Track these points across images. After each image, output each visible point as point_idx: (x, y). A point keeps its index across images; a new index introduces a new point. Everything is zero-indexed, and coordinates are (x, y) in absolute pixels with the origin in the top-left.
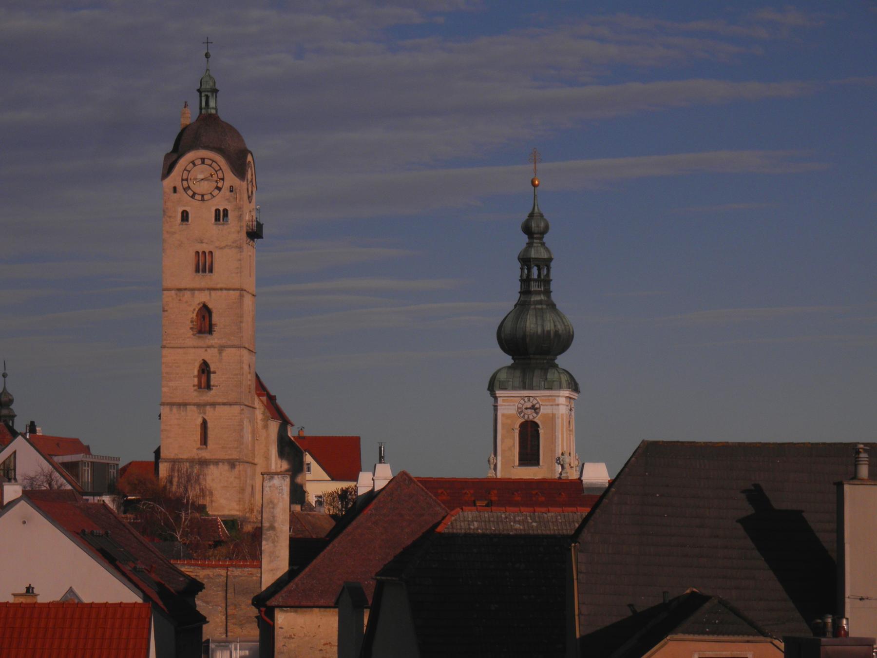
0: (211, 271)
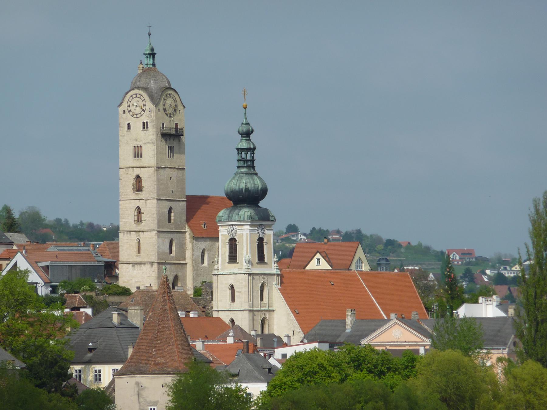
0: (141, 157)
